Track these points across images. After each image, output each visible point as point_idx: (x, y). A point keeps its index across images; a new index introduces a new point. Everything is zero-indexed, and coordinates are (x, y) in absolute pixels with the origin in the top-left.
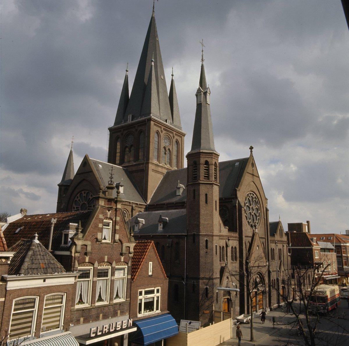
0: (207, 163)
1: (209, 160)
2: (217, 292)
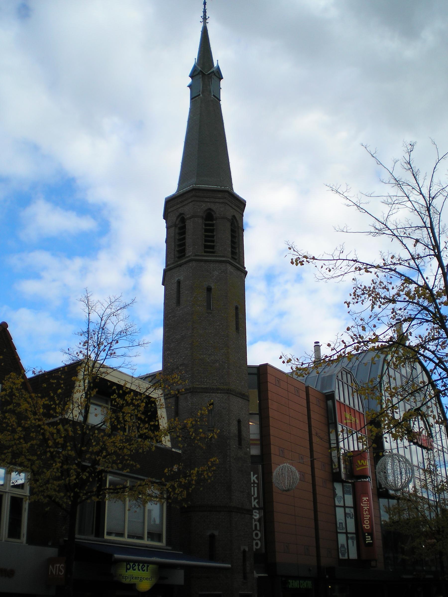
0: (209, 216)
1: (214, 207)
2: (244, 551)
